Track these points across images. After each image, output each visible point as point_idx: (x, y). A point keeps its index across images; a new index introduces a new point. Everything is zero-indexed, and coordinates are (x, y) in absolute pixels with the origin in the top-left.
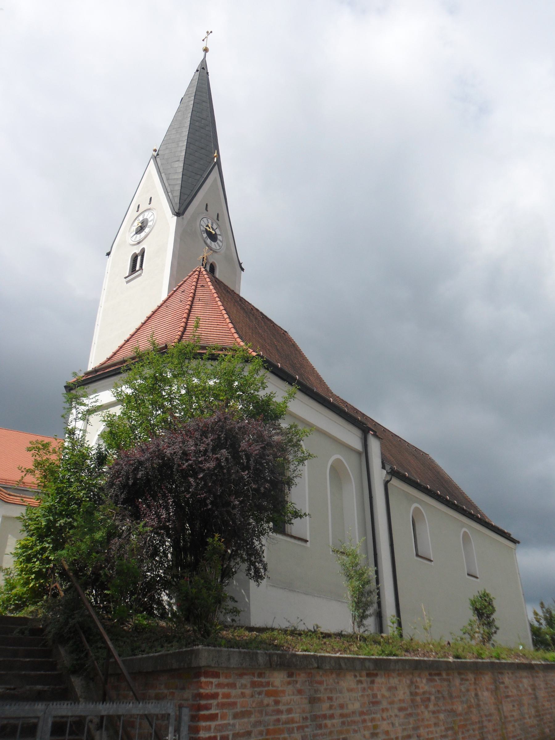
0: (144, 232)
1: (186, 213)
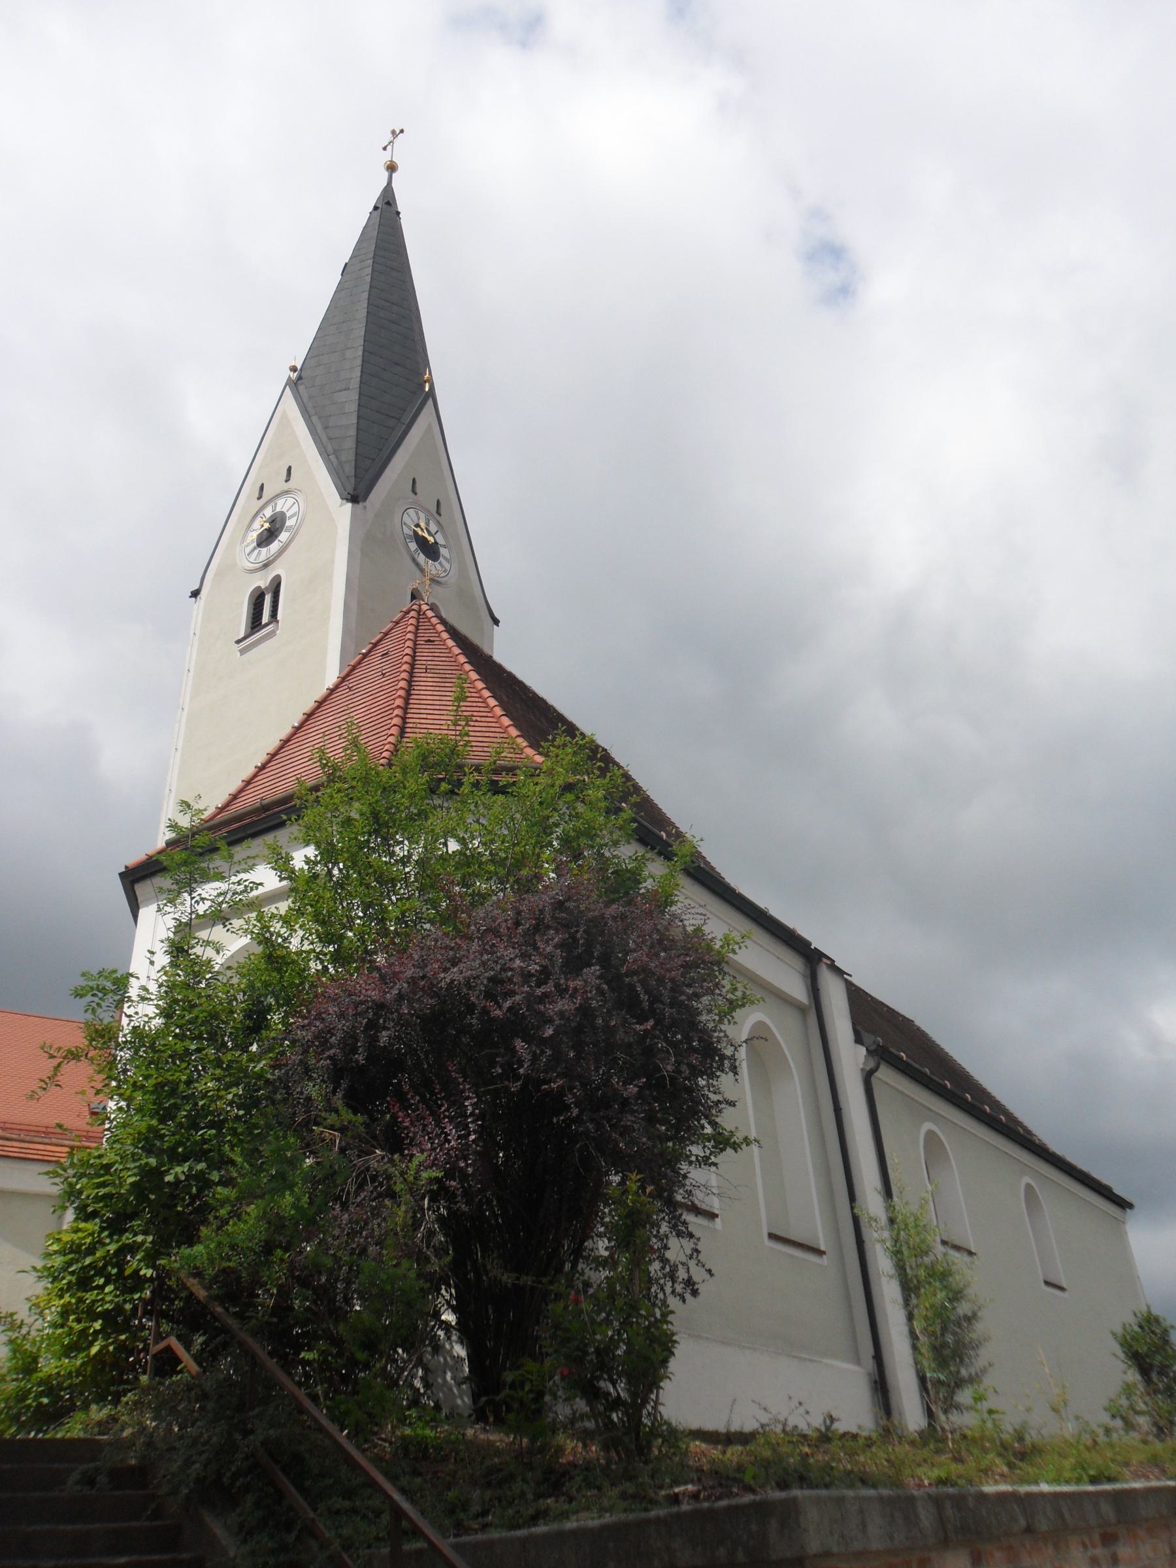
0: (277, 541)
1: (372, 496)
